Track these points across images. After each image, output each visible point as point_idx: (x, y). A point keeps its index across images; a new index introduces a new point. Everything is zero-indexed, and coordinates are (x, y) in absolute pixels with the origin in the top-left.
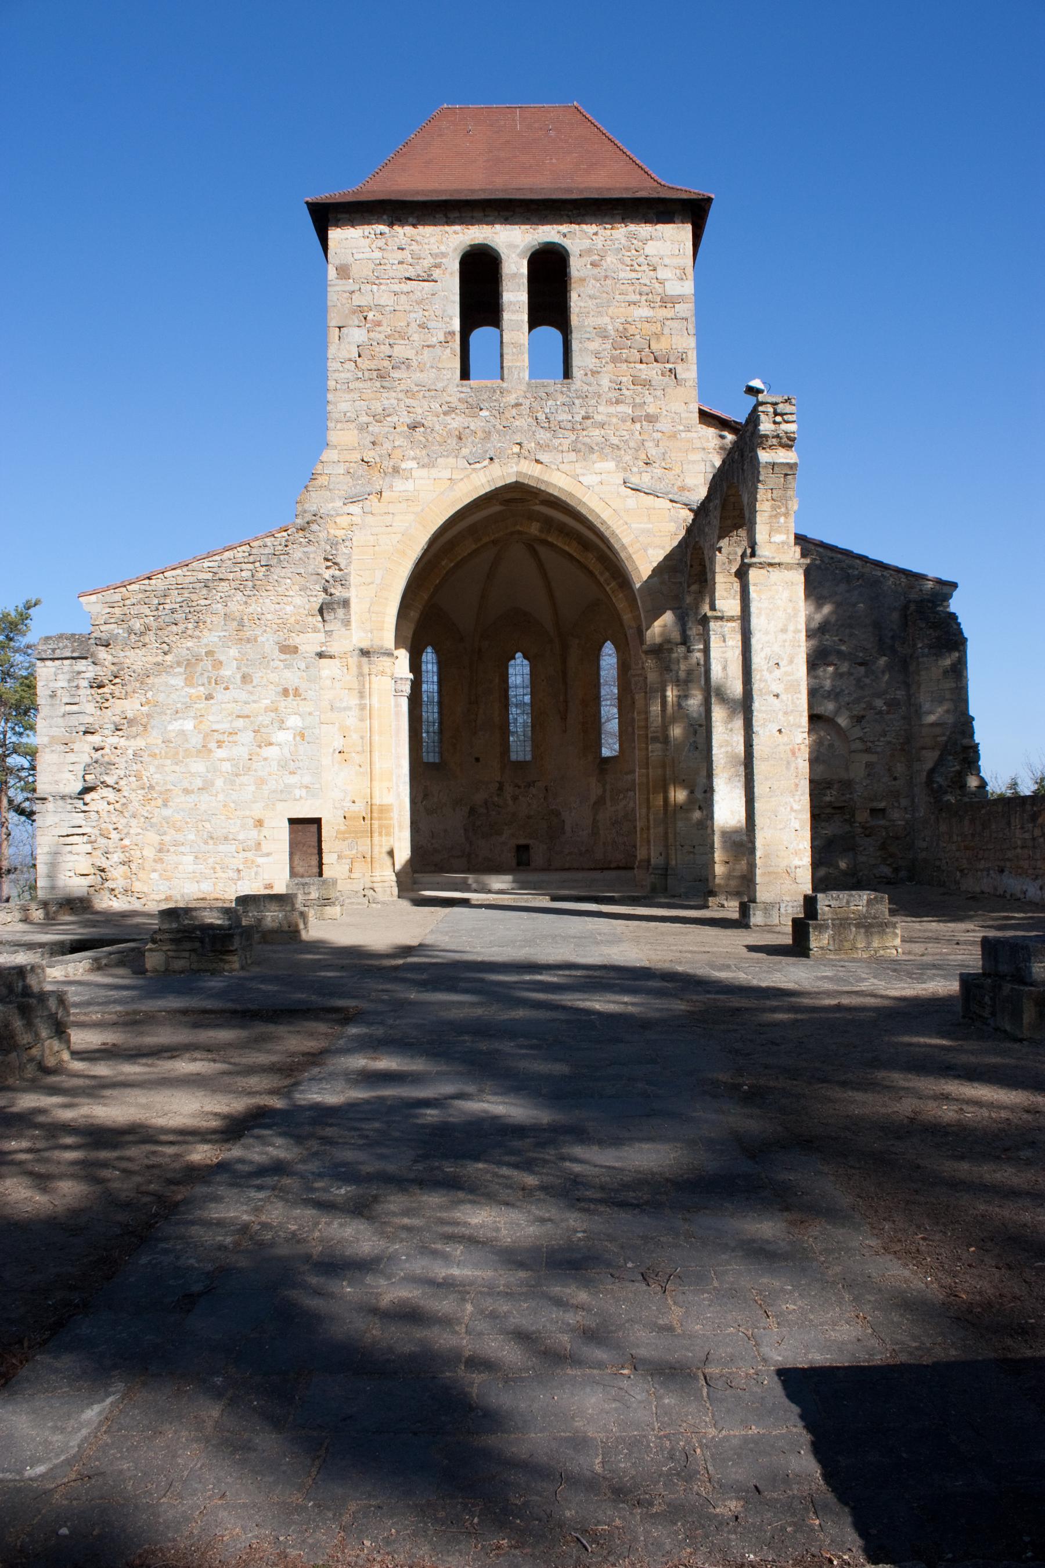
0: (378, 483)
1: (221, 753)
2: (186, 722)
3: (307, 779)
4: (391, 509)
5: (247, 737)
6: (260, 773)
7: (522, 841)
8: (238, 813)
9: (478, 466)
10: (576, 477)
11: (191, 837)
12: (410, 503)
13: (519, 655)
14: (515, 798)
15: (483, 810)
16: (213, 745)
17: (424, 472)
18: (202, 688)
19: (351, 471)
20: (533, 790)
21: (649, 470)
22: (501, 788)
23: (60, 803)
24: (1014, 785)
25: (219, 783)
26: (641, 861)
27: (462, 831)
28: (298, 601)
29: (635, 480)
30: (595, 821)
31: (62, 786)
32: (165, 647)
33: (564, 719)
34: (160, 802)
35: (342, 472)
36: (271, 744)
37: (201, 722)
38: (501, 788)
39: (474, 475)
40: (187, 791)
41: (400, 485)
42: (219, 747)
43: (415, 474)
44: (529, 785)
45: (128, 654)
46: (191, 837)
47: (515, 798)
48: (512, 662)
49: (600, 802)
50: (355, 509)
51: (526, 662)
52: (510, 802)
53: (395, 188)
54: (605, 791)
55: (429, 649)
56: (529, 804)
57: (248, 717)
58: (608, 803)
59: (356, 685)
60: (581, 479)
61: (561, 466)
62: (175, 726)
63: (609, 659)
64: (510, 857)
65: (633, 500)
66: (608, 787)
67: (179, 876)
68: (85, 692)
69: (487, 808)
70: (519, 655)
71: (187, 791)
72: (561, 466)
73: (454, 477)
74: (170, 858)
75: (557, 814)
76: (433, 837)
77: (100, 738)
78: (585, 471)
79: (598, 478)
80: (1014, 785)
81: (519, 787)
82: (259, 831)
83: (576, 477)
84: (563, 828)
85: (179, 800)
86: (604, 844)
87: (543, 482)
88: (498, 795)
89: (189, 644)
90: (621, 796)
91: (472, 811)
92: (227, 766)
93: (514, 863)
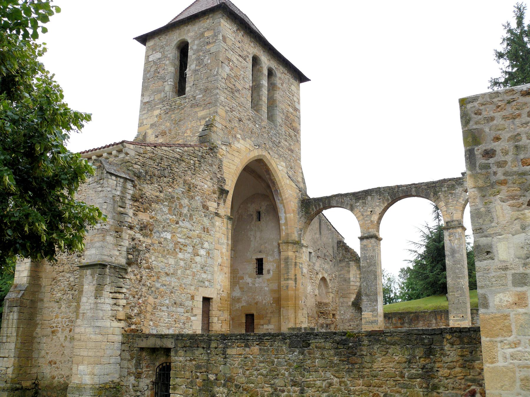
1: (180, 255)
2: (168, 234)
3: (209, 277)
5: (190, 249)
6: (194, 270)
8: (185, 290)
11: (167, 302)
16: (178, 250)
18: (174, 217)
23: (113, 270)
24: (78, 119)
25: (179, 272)
28: (209, 183)
31: (114, 259)
32: (161, 189)
34: (155, 278)
36: (198, 255)
37: (174, 236)
40: (167, 274)
42: (180, 252)
45: (145, 186)
46: (167, 302)
53: (274, 165)
57: (191, 238)
59: (226, 233)
62: (164, 235)
67: (161, 324)
68: (129, 203)
71: (167, 274)
74: (158, 313)
77: (134, 233)
80: (78, 119)
82: (193, 302)
83: (277, 165)
85: (164, 279)
87: (270, 162)
89: (170, 190)
92: (182, 263)
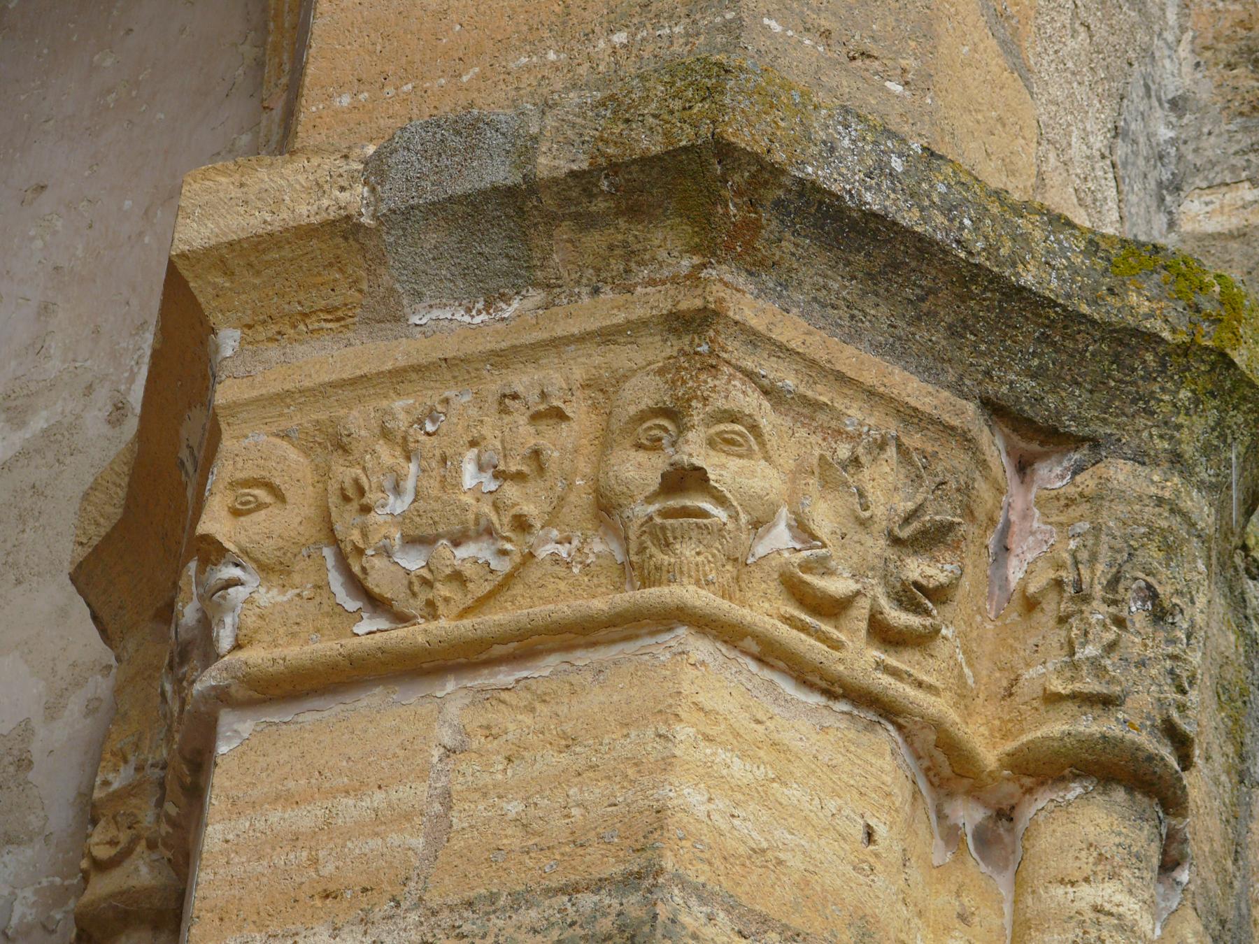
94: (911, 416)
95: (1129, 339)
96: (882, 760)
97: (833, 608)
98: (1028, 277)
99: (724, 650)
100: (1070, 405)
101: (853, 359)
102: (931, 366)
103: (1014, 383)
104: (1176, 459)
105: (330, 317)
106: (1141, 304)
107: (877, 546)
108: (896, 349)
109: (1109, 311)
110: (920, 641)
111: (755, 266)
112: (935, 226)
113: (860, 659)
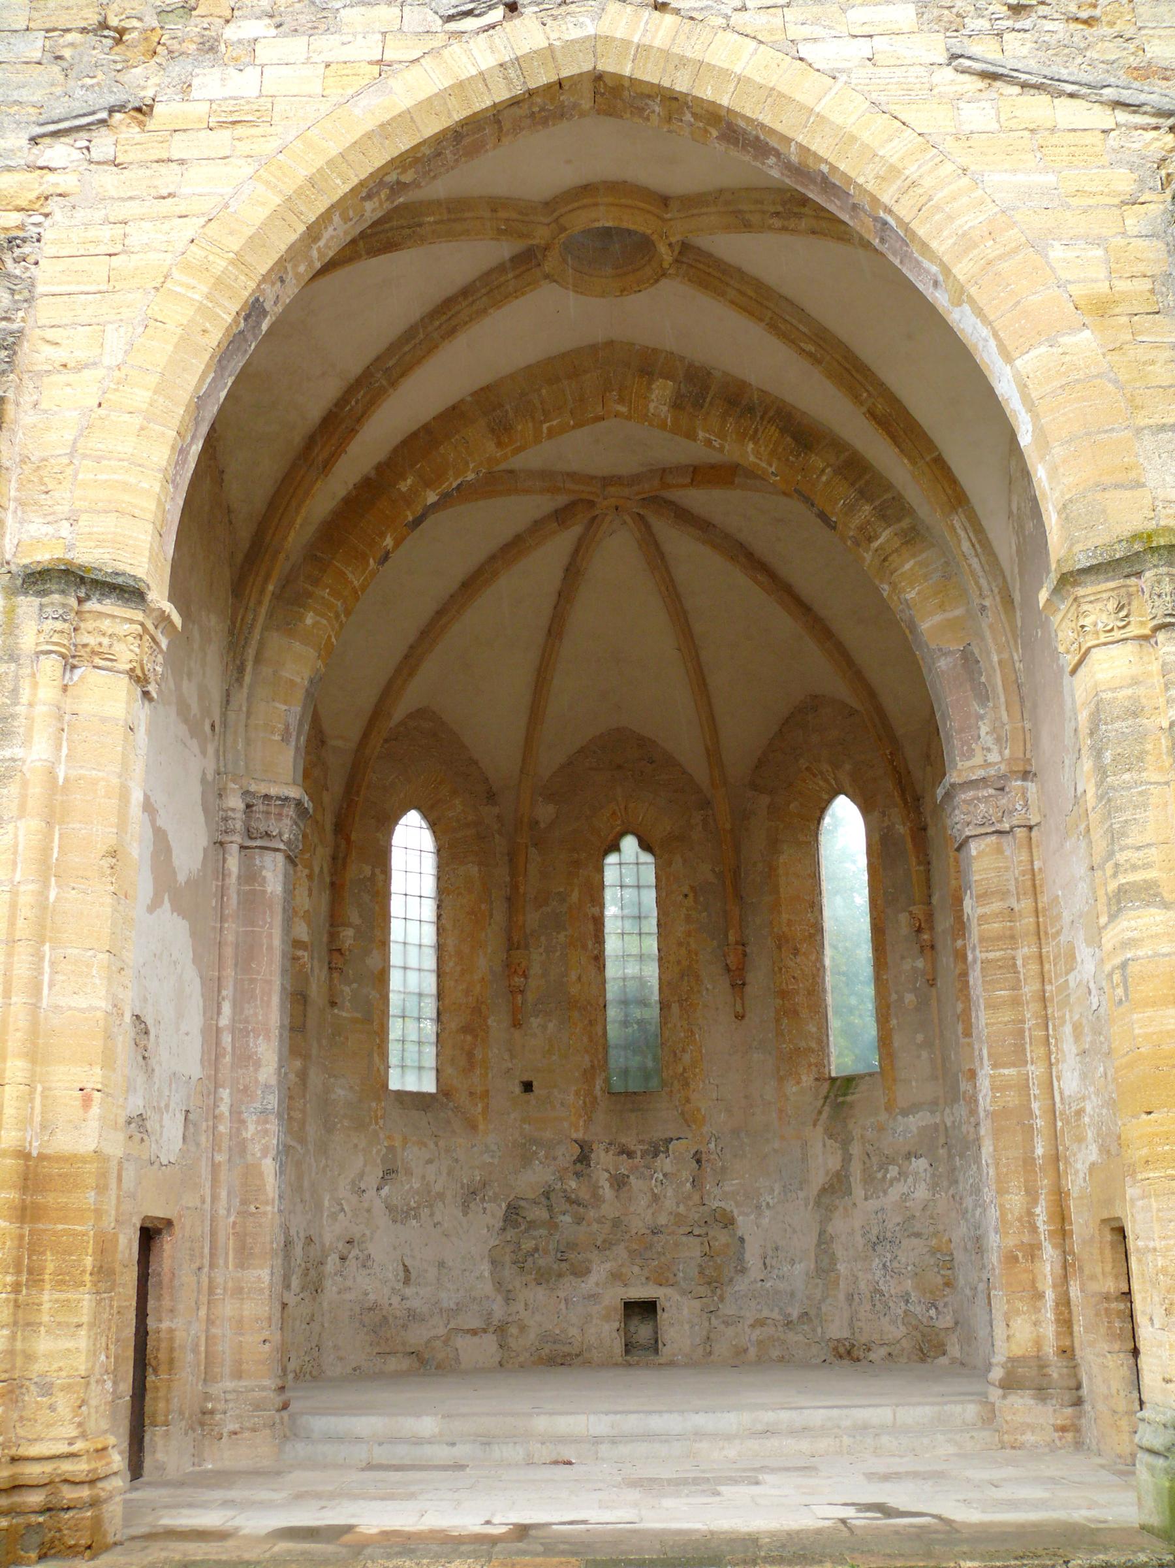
0: (144, 80)
4: (179, 147)
7: (640, 1292)
9: (469, 24)
10: (792, 50)
12: (240, 130)
13: (629, 844)
14: (620, 1183)
15: (540, 1213)
17: (296, 46)
19: (67, 53)
20: (665, 1163)
21: (1026, 23)
22: (584, 1158)
26: (1013, 1362)
27: (485, 1268)
29: (986, 50)
30: (824, 1242)
33: (738, 985)
35: (37, 55)
38: (584, 1158)
39: (456, 48)
41: (213, 84)
43: (264, 53)
44: (656, 1150)
47: (620, 1183)
48: (612, 859)
49: (836, 1187)
50: (59, 153)
51: (647, 858)
52: (607, 1192)
54: (847, 1159)
55: (413, 818)
56: (656, 1198)
58: (858, 1191)
60: (805, 50)
61: (738, 19)
63: (845, 831)
64: (606, 1332)
65: (983, 110)
66: (856, 1149)
69: (550, 1208)
70: (629, 844)
72: (738, 19)
73: (388, 57)
75: (727, 1222)
76: (407, 1281)
78: (818, 31)
79: (863, 48)
81: (630, 1155)
83: (792, 50)
84: (741, 1260)
86: (850, 1298)
87: (683, 62)
88: (578, 1175)
90: (893, 1171)
91: (513, 1215)
93: (618, 1346)
94: (1113, 589)
95: (1137, 553)
96: (1130, 646)
97: (1112, 630)
98: (1117, 556)
99: (271, 531)
100: (1137, 568)
101: (1103, 586)
102: (1113, 579)
103: (1127, 570)
104: (1155, 566)
105: (934, 1536)
106: (1138, 547)
107: (1113, 616)
108: (1107, 580)
109: (1133, 551)
110: (1129, 623)
111: (1079, 585)
112: (1100, 560)
113: (1118, 635)
